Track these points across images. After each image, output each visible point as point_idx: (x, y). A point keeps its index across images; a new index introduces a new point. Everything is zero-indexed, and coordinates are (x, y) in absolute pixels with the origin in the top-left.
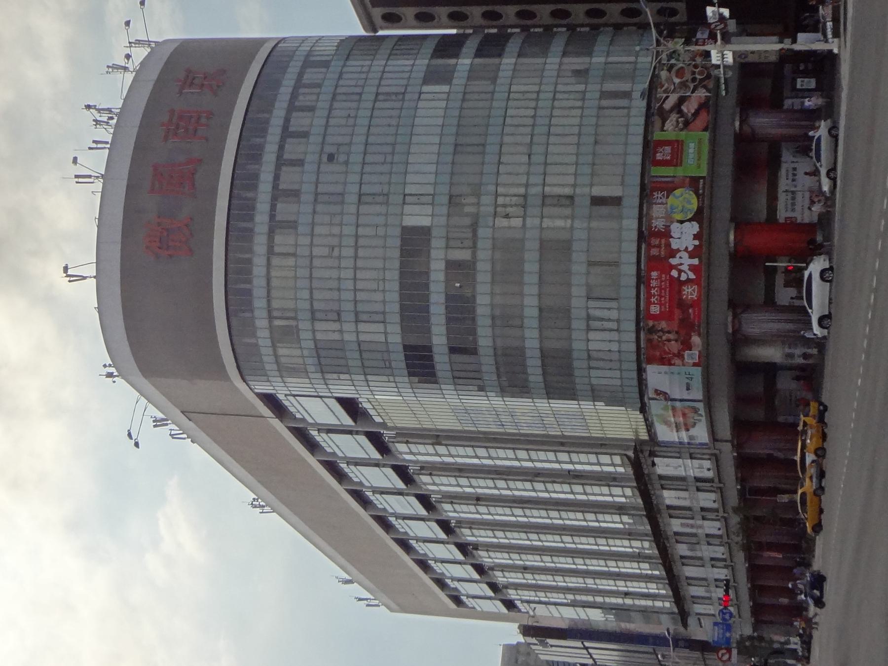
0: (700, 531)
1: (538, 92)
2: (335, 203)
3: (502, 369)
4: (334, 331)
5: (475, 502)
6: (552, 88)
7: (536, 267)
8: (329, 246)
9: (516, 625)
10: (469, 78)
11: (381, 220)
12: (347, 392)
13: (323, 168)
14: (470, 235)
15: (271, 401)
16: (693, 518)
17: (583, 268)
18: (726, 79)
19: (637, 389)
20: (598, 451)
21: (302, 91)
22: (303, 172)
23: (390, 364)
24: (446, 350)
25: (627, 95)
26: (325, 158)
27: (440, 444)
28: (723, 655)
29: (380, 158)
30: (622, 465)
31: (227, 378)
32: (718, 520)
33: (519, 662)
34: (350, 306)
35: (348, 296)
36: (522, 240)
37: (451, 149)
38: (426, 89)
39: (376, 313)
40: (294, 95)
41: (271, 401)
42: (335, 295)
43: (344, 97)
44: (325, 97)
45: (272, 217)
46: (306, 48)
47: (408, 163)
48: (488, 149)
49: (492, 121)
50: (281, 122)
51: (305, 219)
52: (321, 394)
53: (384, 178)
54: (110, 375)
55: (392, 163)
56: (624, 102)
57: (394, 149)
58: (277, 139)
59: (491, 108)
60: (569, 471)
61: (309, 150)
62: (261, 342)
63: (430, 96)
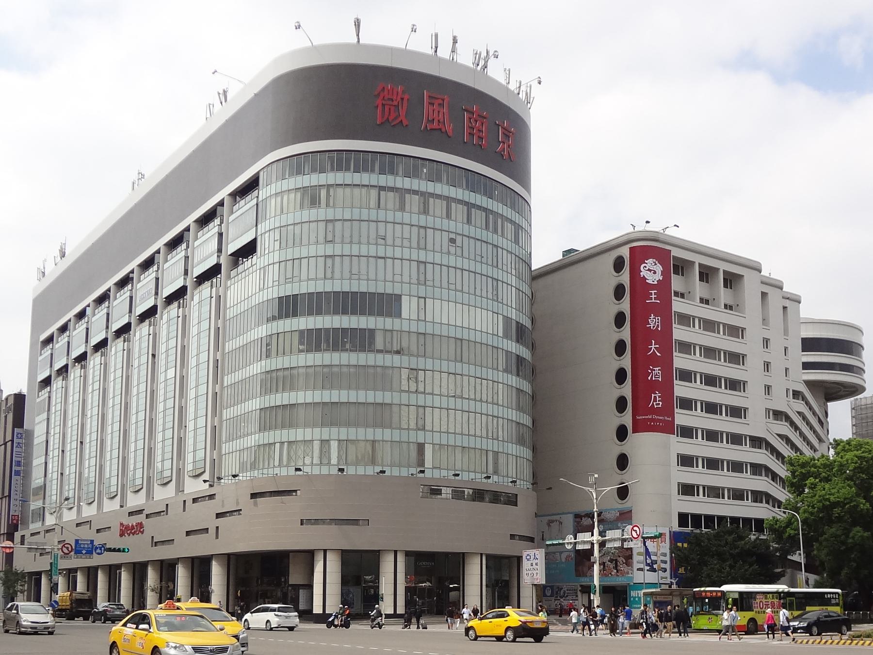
3: (287, 373)
6: (500, 415)
7: (371, 400)
9: (762, 273)
10: (507, 351)
11: (406, 279)
13: (445, 234)
18: (564, 544)
22: (442, 218)
24: (301, 328)
26: (453, 236)
28: (67, 548)
29: (452, 280)
36: (391, 390)
38: (500, 317)
39: (333, 272)
46: (524, 224)
49: (478, 368)
51: (407, 218)
52: (259, 226)
53: (437, 284)
59: (487, 367)
61: (457, 225)
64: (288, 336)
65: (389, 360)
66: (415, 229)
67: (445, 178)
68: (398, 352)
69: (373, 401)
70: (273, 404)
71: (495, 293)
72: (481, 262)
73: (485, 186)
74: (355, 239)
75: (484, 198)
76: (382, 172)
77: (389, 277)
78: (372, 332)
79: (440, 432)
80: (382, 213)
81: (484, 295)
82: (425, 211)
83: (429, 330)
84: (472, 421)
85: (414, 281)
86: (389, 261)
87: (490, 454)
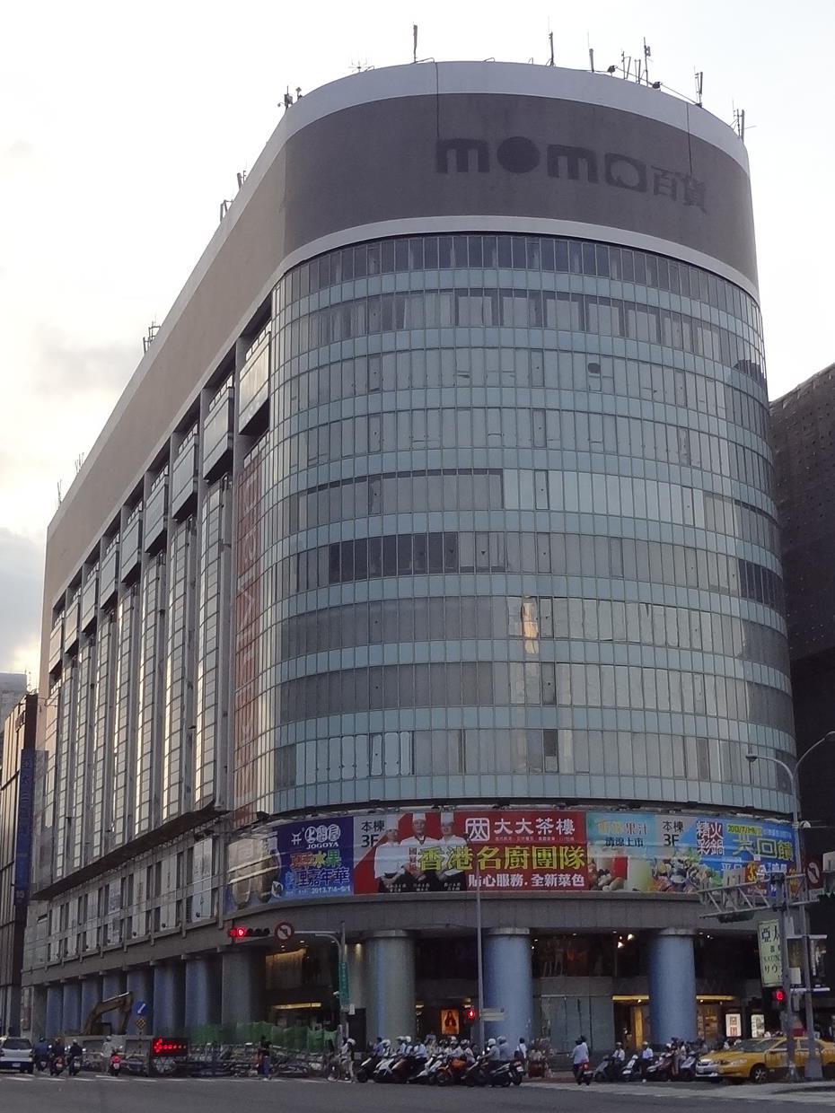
0: (135, 908)
1: (701, 650)
2: (530, 376)
3: (313, 619)
4: (354, 385)
5: (159, 609)
7: (453, 657)
8: (470, 371)
12: (275, 416)
14: (494, 564)
15: (264, 315)
16: (148, 897)
17: (455, 723)
19: (291, 808)
20: (218, 763)
21: (686, 326)
23: (314, 466)
24: (333, 541)
25: (705, 774)
26: (593, 360)
27: (220, 550)
29: (596, 436)
30: (202, 798)
31: (288, 251)
32: (147, 932)
33: (5, 696)
34: (388, 404)
35: (403, 400)
37: (615, 532)
39: (381, 441)
40: (678, 316)
41: (264, 315)
42: (404, 383)
43: (695, 625)
44: (679, 359)
45: (508, 292)
46: (741, 329)
47: (592, 473)
48: (618, 583)
50: (641, 299)
52: (272, 379)
54: (288, 100)
55: (590, 451)
56: (694, 770)
57: (680, 778)
58: (617, 295)
60: (195, 727)
62: (336, 289)
63: (695, 625)
64: (313, 555)
65: (482, 583)
66: (523, 355)
67: (614, 272)
68: (500, 569)
69: (457, 659)
70: (311, 671)
71: (684, 451)
72: (653, 401)
73: (663, 269)
74: (418, 382)
75: (685, 300)
76: (548, 266)
77: (479, 441)
78: (452, 538)
79: (602, 707)
80: (462, 333)
81: (650, 452)
82: (541, 322)
83: (557, 526)
84: (649, 683)
85: (526, 442)
86: (478, 413)
87: (691, 743)
